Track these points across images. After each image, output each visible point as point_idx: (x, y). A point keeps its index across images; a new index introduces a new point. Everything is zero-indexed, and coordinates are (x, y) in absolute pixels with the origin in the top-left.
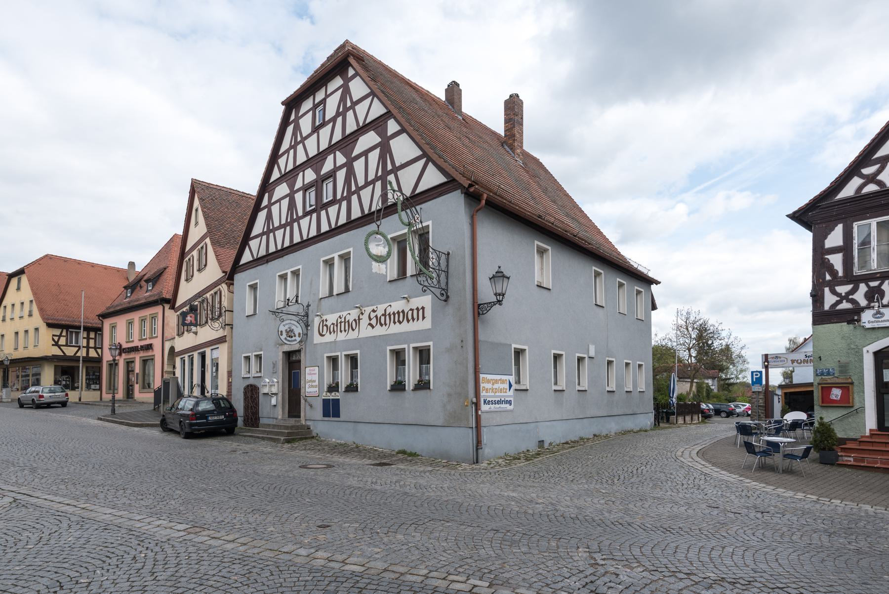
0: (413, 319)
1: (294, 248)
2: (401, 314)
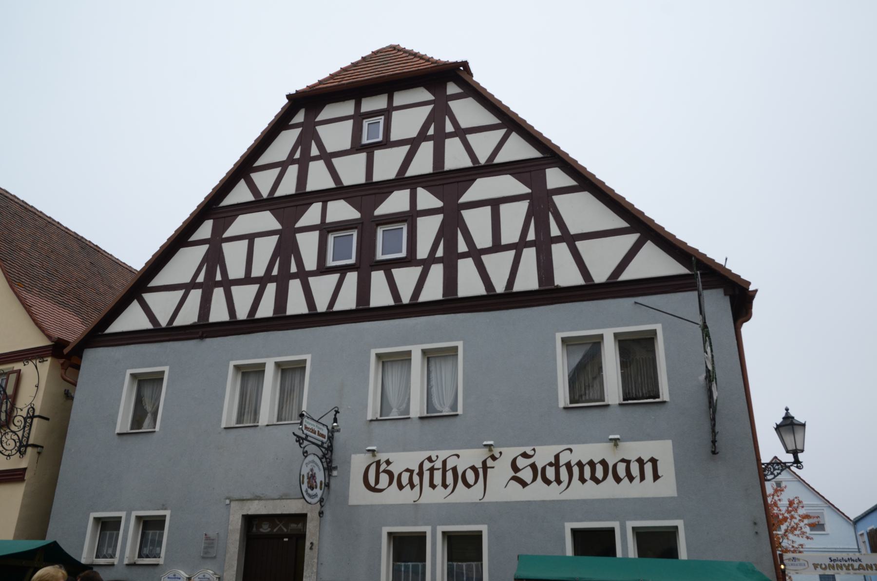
0: (631, 478)
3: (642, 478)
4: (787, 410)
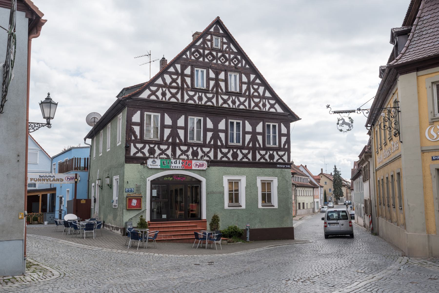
4: (49, 94)
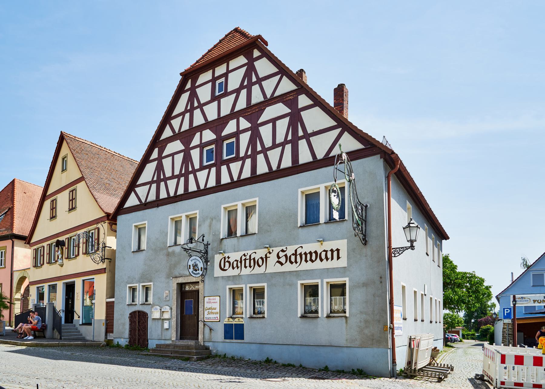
0: (327, 259)
1: (188, 196)
2: (314, 255)
3: (332, 259)
